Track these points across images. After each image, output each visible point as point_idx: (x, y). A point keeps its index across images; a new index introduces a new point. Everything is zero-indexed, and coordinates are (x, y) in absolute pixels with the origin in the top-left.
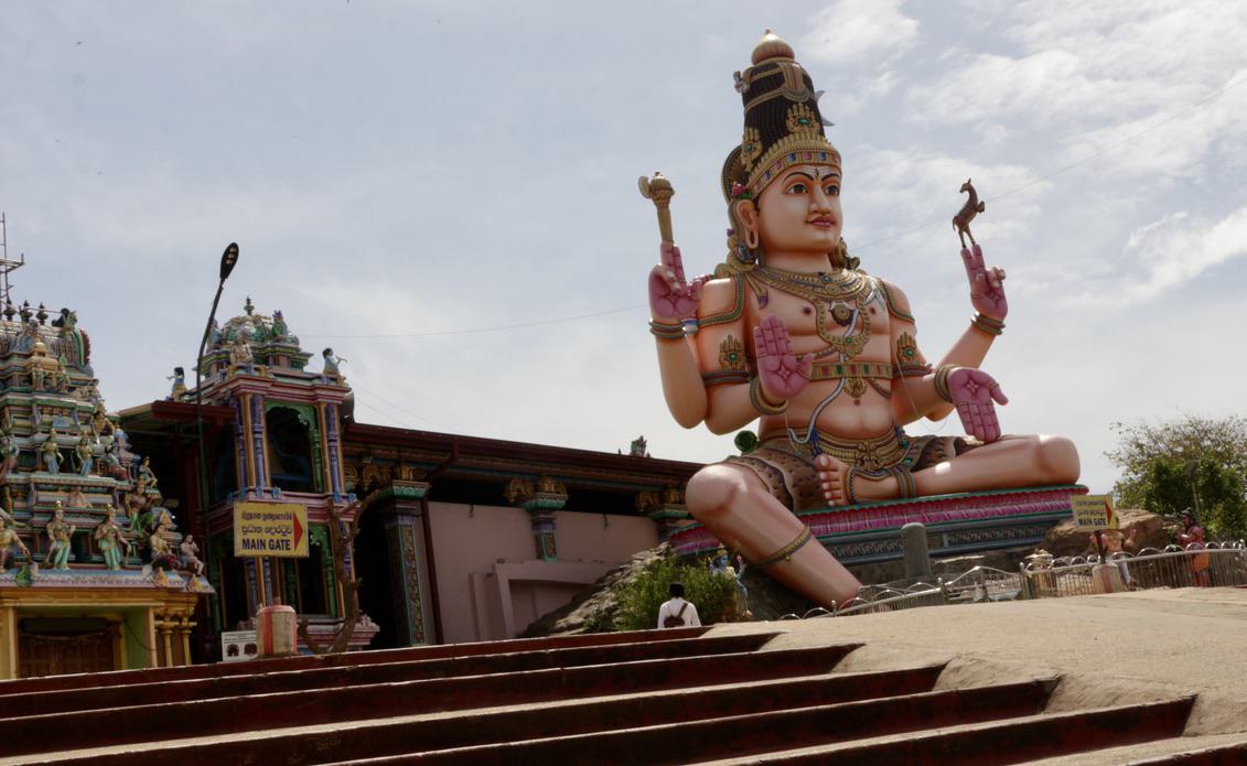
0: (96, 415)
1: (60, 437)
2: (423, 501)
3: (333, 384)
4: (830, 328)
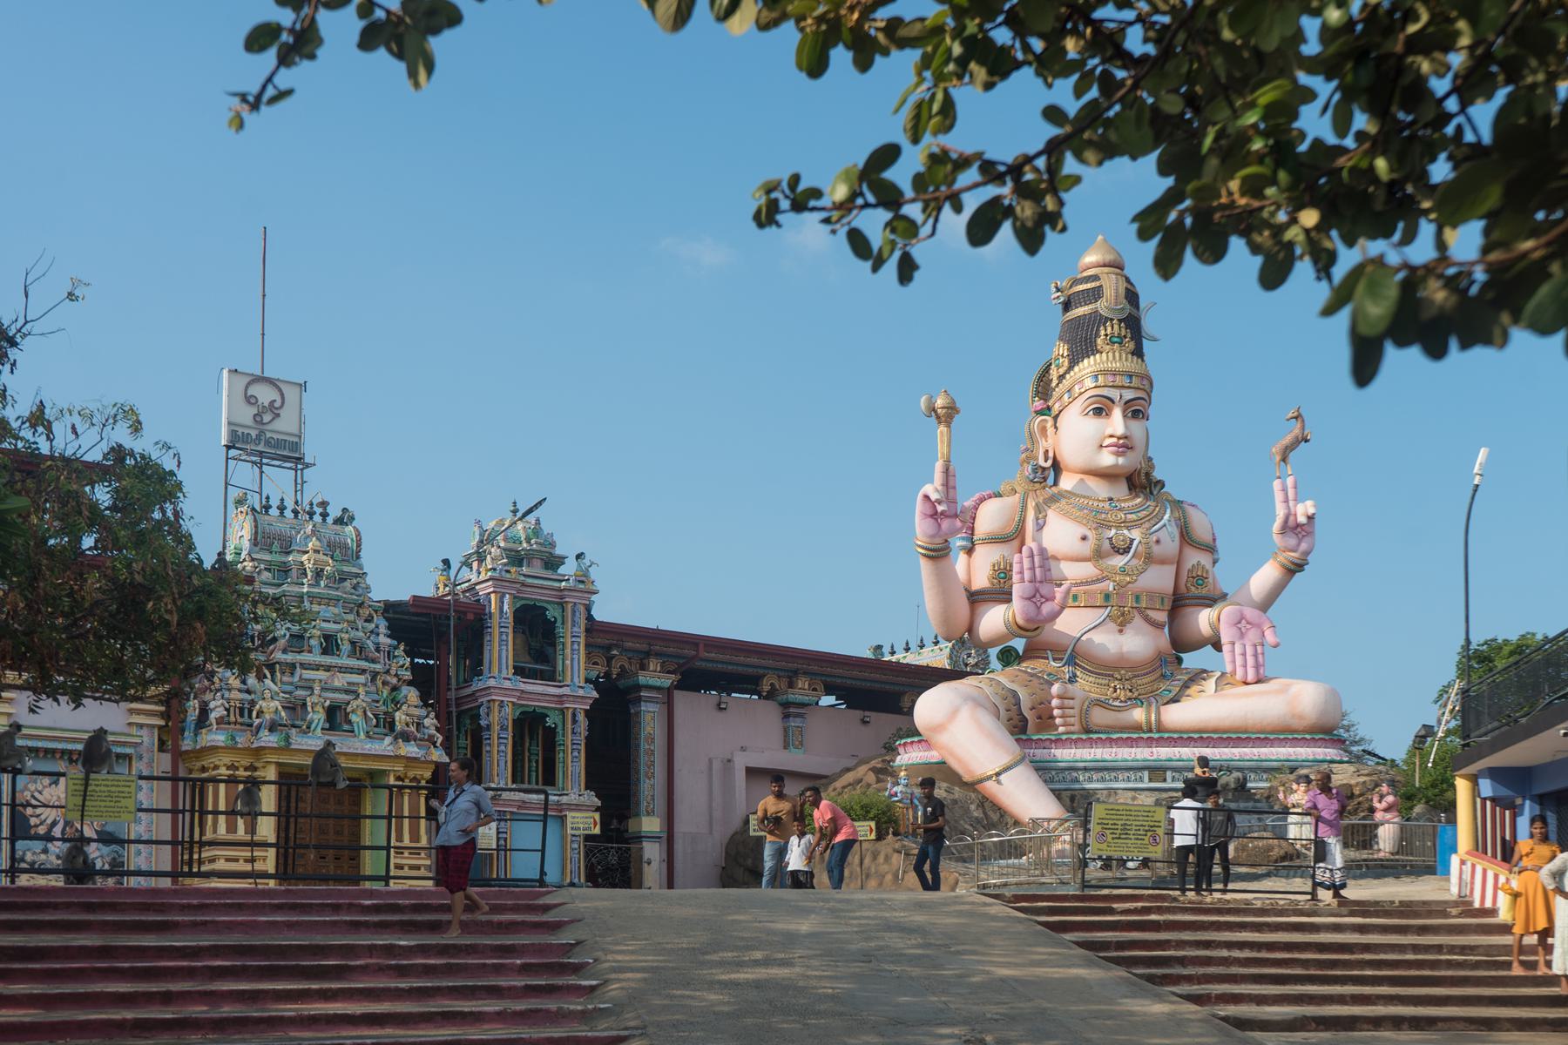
0: (361, 605)
2: (669, 692)
3: (581, 586)
4: (1108, 555)
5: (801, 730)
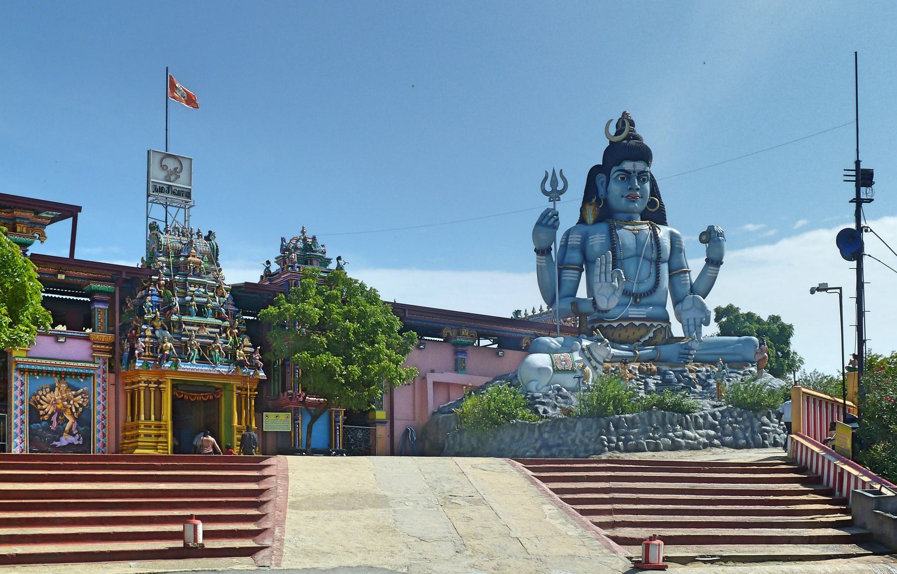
1: (196, 299)
5: (464, 360)
